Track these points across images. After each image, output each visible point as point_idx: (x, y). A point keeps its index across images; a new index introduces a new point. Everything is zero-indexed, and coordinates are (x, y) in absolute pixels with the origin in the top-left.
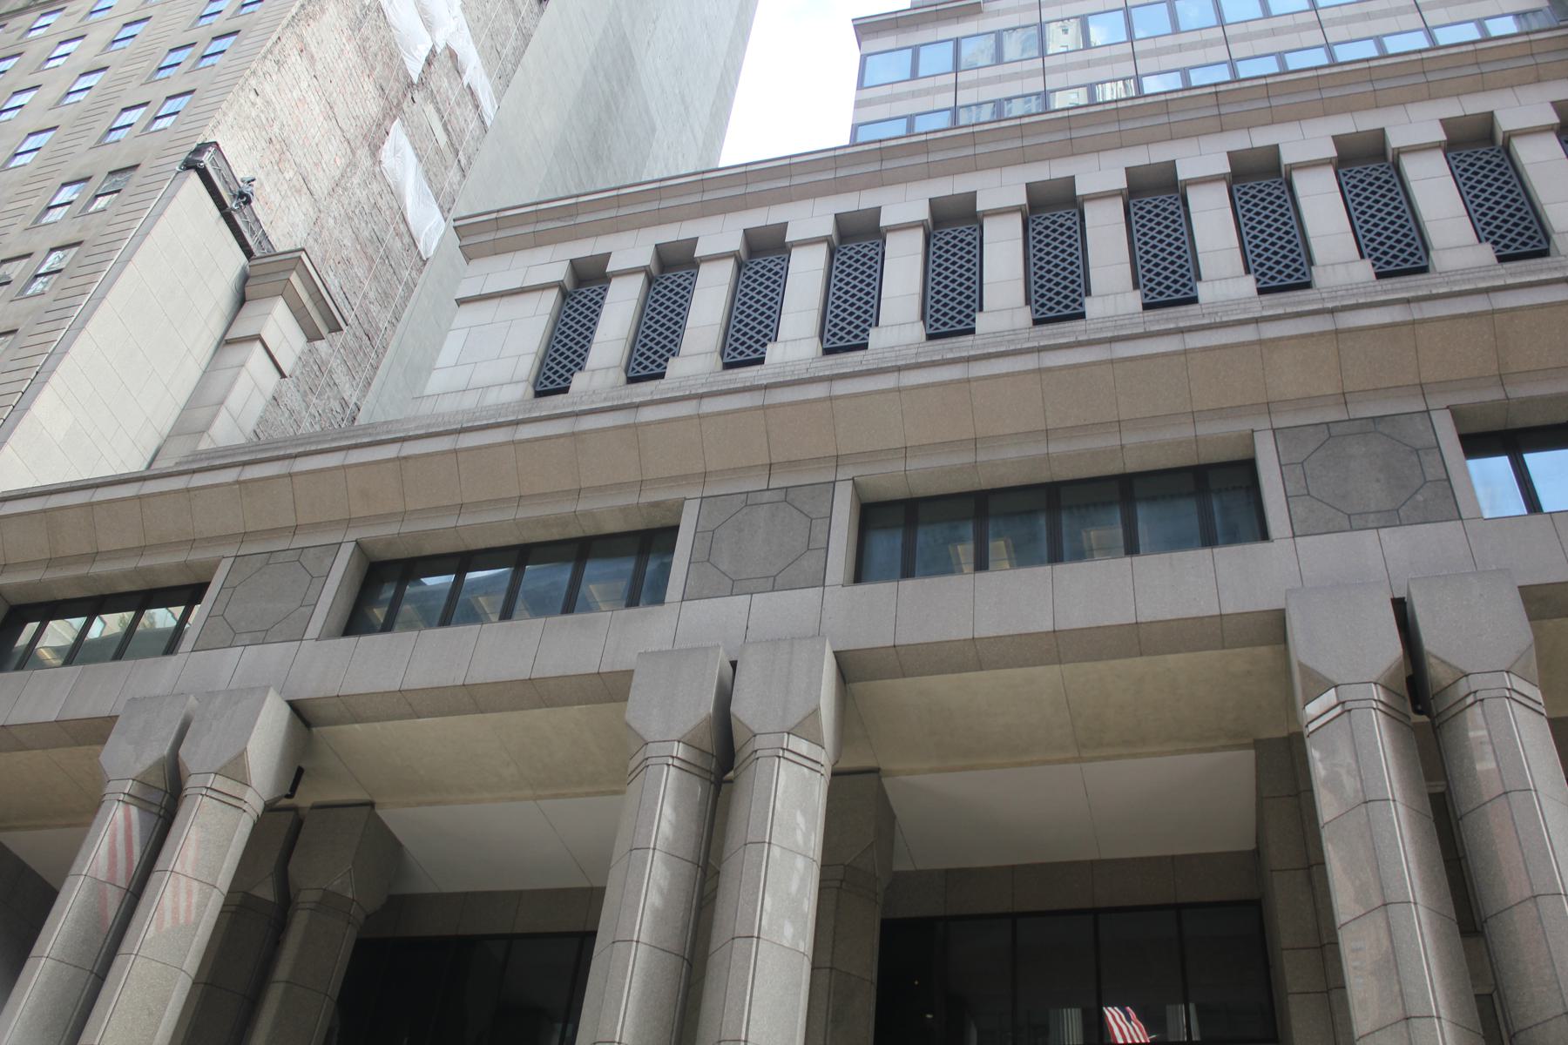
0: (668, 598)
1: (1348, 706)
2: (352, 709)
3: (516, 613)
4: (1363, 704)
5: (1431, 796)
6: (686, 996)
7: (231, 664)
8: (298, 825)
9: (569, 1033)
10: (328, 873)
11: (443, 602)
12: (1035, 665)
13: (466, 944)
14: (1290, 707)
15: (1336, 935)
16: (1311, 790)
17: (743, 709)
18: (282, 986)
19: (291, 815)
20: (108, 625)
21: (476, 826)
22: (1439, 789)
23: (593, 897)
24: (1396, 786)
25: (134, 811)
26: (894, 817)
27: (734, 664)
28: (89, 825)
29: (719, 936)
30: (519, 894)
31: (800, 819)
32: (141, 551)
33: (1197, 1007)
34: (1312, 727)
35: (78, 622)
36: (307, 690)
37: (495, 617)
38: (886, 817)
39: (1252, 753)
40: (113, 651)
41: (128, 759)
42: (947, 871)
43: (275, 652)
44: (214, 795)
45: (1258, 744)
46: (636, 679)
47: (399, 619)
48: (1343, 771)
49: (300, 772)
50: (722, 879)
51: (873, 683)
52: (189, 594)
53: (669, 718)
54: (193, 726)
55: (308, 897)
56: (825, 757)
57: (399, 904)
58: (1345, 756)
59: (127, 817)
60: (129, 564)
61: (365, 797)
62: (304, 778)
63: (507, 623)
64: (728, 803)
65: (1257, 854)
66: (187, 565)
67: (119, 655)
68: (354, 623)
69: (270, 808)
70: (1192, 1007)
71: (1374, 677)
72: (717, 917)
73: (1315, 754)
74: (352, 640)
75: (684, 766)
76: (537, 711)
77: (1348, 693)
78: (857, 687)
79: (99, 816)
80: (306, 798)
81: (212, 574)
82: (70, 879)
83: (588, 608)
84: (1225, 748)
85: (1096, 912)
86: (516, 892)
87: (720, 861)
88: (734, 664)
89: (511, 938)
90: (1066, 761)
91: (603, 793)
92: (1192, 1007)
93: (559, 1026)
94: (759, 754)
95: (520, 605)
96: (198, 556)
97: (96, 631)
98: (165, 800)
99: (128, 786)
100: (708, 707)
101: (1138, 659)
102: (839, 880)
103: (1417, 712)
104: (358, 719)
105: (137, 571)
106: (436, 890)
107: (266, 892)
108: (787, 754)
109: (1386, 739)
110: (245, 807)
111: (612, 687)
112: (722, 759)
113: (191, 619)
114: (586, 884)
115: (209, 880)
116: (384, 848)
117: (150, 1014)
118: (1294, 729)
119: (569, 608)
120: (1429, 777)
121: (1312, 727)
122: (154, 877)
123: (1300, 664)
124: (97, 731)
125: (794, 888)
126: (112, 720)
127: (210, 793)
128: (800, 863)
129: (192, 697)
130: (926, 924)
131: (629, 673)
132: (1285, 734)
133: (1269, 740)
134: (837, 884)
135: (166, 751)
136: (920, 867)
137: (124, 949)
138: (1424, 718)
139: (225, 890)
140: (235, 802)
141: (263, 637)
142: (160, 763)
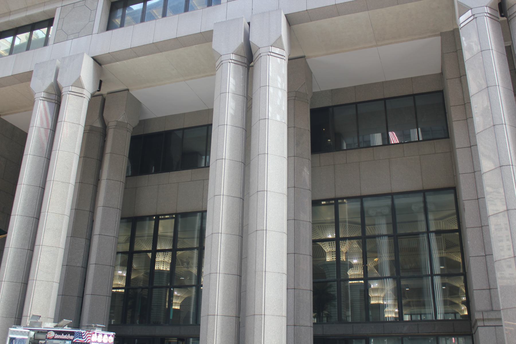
0: (222, 2)
1: (475, 16)
2: (116, 56)
3: (168, 15)
4: (481, 15)
5: (506, 47)
6: (246, 141)
7: (69, 46)
8: (104, 101)
9: (207, 160)
10: (116, 115)
11: (140, 14)
12: (359, 12)
13: (167, 135)
14: (454, 19)
15: (470, 100)
16: (461, 49)
17: (254, 39)
18: (109, 154)
19: (101, 97)
20: (22, 38)
21: (165, 99)
22: (509, 45)
23: (210, 112)
24: (493, 44)
25: (46, 103)
26: (312, 73)
27: (249, 24)
28: (32, 110)
29: (254, 120)
30: (184, 114)
31: (279, 79)
32: (26, 9)
33: (422, 131)
34: (462, 25)
35: (10, 39)
36: (97, 53)
37: (160, 17)
38: (309, 73)
39: (440, 38)
40: (25, 48)
41: (40, 85)
42: (332, 90)
43: (84, 40)
44: (73, 93)
45: (442, 34)
46: (215, 33)
47: (126, 22)
48: (473, 44)
49: (101, 82)
50: (254, 100)
51: (300, 25)
52: (48, 23)
53: (228, 45)
54: (60, 70)
55: (111, 124)
56: (285, 53)
57: (143, 123)
58: (475, 39)
59: (44, 105)
60: (23, 15)
61: (125, 88)
62: (103, 84)
63: (165, 18)
64: (252, 74)
65: (442, 74)
66: (44, 12)
67: (28, 49)
68: (110, 26)
69: (93, 96)
70: (419, 129)
71: (486, 4)
72: (253, 114)
73: (463, 39)
74: (110, 32)
75: (235, 62)
76: (181, 49)
77: (475, 11)
78: (293, 27)
79: (35, 106)
80: (104, 91)
81: (54, 14)
82: (30, 129)
83: (194, 9)
84: (429, 36)
85: (385, 99)
86: (183, 114)
87: (252, 95)
88: (249, 24)
89: (184, 129)
90: (372, 47)
91: (208, 76)
92: (419, 129)
93: (204, 157)
94: (261, 55)
95: (168, 11)
96: (48, 8)
97: (17, 42)
98: (56, 98)
99: (43, 94)
100: (241, 40)
101: (397, 6)
102: (294, 96)
103: (502, 16)
104: (117, 60)
105: (27, 17)
106: (155, 117)
107: (98, 124)
108: (272, 54)
109: (490, 27)
110: (84, 96)
111: (206, 37)
112: (249, 58)
113: (51, 33)
114: (207, 108)
115: (77, 123)
116: (135, 104)
117: (68, 168)
118: (455, 27)
119: (186, 10)
120: (505, 40)
121: (462, 25)
122: (58, 124)
123: (458, 2)
124: (27, 77)
125: (278, 103)
126: (31, 72)
127: (71, 93)
128: (280, 93)
129: (57, 60)
130: (325, 109)
131: (212, 31)
132: (452, 29)
133: (446, 32)
134: (294, 98)
135: (53, 80)
136: (322, 89)
137: (54, 148)
138: (505, 18)
139: (84, 125)
140: (80, 95)
141: (78, 35)
142: (51, 85)
